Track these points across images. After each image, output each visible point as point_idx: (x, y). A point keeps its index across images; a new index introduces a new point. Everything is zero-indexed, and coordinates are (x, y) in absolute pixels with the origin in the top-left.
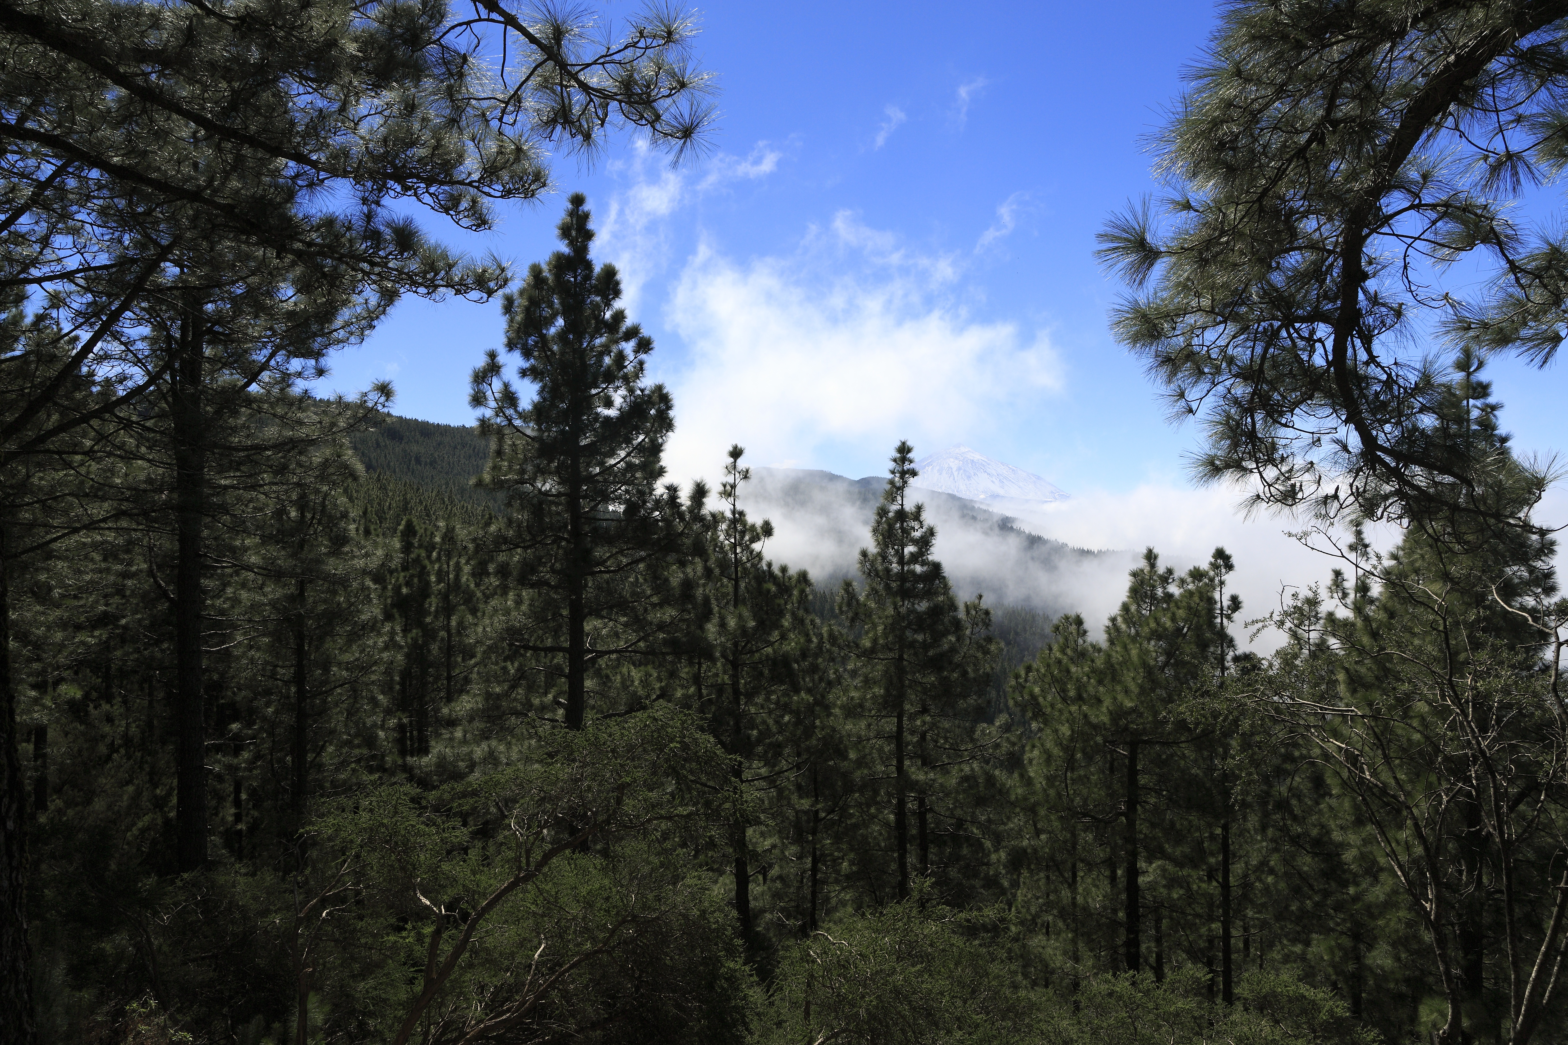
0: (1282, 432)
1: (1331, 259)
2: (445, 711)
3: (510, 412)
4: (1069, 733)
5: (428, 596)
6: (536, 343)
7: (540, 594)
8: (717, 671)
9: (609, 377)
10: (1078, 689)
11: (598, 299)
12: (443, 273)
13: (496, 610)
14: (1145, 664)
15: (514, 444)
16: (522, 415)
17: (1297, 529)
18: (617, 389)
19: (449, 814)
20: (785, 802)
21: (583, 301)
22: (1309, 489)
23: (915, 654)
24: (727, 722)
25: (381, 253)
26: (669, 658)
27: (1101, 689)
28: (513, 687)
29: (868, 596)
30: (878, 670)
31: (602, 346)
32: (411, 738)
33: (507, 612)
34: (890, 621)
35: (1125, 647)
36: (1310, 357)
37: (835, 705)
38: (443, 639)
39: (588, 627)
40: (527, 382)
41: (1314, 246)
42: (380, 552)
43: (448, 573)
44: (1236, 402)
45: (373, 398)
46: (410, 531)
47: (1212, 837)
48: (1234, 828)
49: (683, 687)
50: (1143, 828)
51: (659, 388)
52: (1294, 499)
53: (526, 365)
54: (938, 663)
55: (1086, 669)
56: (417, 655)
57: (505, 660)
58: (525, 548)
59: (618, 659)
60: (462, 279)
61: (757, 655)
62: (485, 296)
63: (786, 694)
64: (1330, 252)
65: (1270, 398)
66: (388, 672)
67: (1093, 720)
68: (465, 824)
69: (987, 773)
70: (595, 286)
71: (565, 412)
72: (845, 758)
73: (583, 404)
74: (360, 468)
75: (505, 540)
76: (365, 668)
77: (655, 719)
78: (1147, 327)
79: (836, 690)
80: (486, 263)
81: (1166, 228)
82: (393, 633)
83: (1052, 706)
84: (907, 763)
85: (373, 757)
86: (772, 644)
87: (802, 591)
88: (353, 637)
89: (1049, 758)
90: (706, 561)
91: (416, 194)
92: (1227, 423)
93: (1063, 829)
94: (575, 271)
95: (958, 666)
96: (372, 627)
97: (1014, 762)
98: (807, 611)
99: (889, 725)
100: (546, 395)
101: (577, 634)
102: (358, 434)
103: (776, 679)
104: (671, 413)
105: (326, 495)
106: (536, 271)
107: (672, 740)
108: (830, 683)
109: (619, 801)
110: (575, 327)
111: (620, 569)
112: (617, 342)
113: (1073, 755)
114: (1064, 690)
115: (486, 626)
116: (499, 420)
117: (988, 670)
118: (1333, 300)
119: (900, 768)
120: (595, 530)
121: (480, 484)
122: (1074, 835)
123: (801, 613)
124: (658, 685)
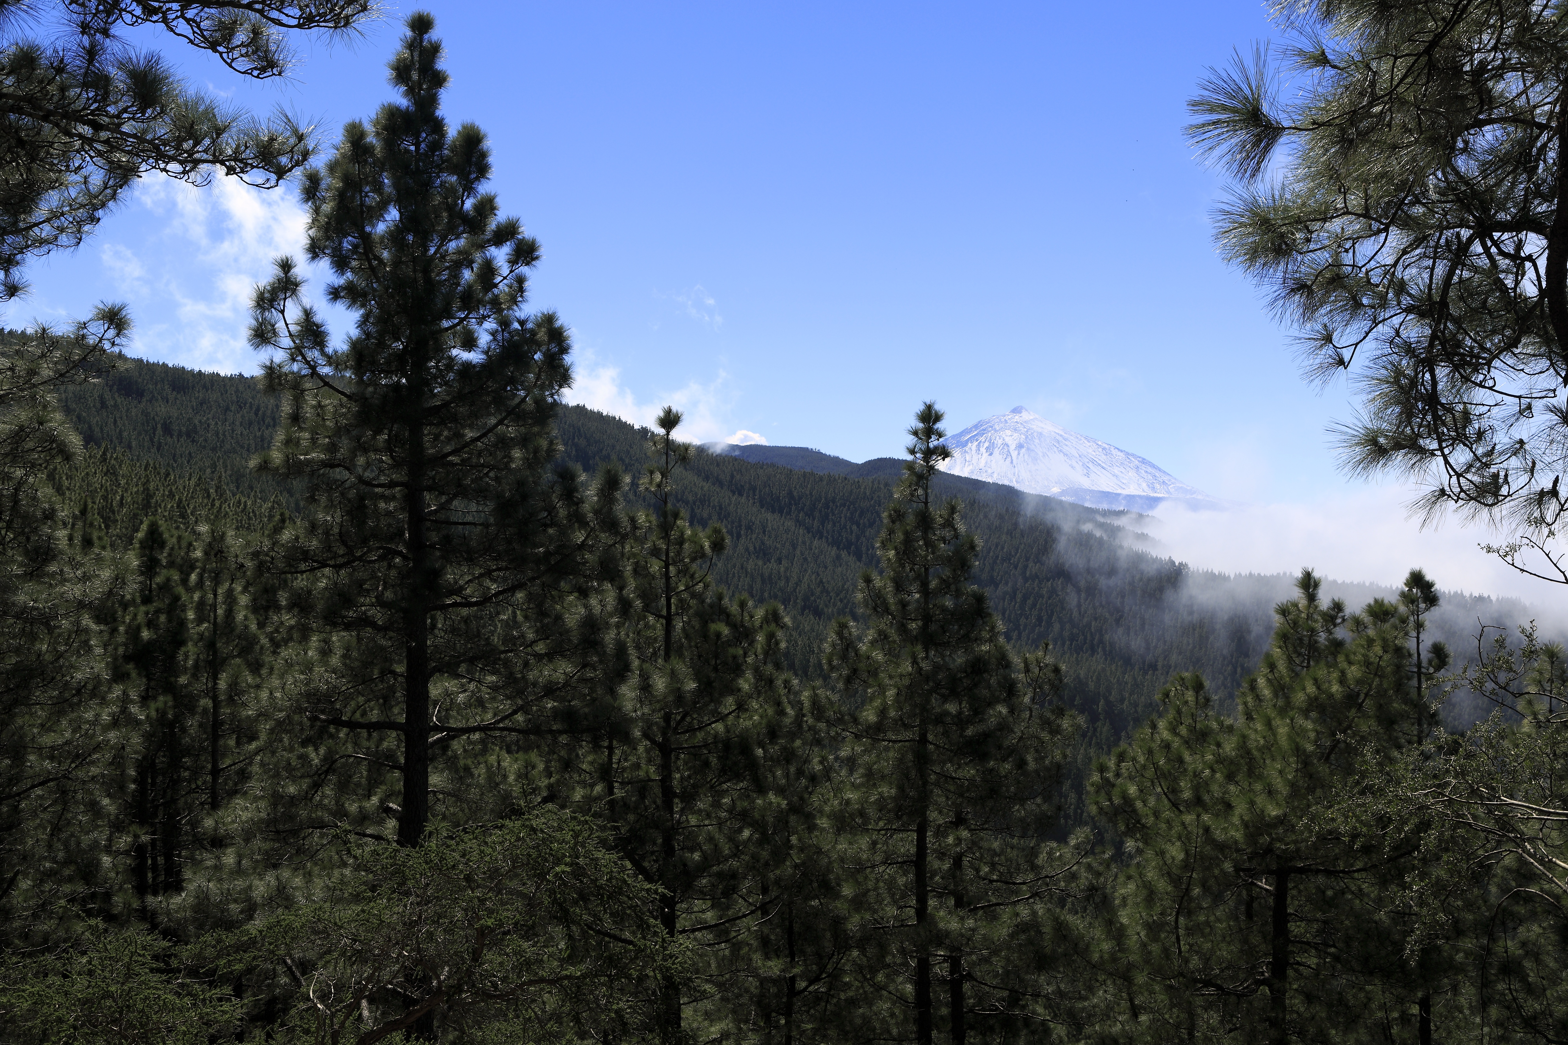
0: (1480, 395)
1: (1544, 137)
2: (209, 823)
3: (313, 354)
4: (1182, 856)
5: (182, 643)
6: (355, 246)
7: (359, 639)
8: (639, 760)
9: (469, 301)
10: (1196, 789)
11: (454, 179)
12: (207, 142)
13: (289, 664)
14: (1298, 750)
15: (319, 405)
16: (330, 360)
17: (1500, 541)
18: (482, 320)
19: (212, 979)
20: (742, 965)
21: (427, 184)
22: (1518, 481)
23: (946, 734)
24: (646, 833)
25: (112, 110)
26: (563, 739)
27: (1232, 788)
28: (316, 786)
29: (873, 643)
30: (887, 759)
31: (459, 252)
32: (155, 867)
33: (308, 667)
34: (906, 681)
35: (1268, 723)
36: (1517, 283)
37: (821, 812)
38: (205, 710)
39: (435, 690)
40: (340, 307)
41: (1521, 118)
42: (106, 574)
43: (214, 607)
44: (1409, 349)
45: (96, 331)
46: (154, 540)
47: (1405, 1019)
48: (1439, 1006)
49: (583, 784)
50: (1295, 1002)
51: (549, 320)
52: (1496, 494)
53: (339, 281)
54: (978, 749)
55: (1209, 757)
56: (165, 736)
57: (304, 744)
58: (337, 567)
59: (482, 741)
60: (236, 151)
61: (700, 735)
62: (273, 177)
63: (745, 795)
64: (1542, 127)
65: (1459, 344)
66: (118, 761)
67: (1219, 835)
68: (239, 992)
69: (1056, 919)
70: (449, 160)
71: (400, 357)
72: (837, 896)
73: (426, 344)
74: (74, 440)
75: (306, 555)
76: (81, 758)
77: (534, 830)
78: (1270, 237)
79: (825, 789)
80: (274, 127)
81: (1291, 92)
82: (125, 700)
83: (1156, 814)
84: (932, 903)
85: (93, 896)
86: (722, 718)
87: (771, 636)
88: (63, 706)
89: (1150, 896)
90: (621, 589)
91: (165, 21)
92: (1397, 381)
93: (1172, 1006)
94: (418, 136)
95: (1012, 751)
96: (93, 690)
97: (1098, 901)
98: (778, 666)
99: (905, 844)
100: (371, 329)
101: (418, 701)
102: (71, 388)
103: (729, 772)
104: (568, 359)
105: (21, 483)
106: (355, 134)
107: (558, 861)
108: (813, 779)
109: (476, 956)
110: (416, 224)
111: (486, 600)
112: (482, 247)
113: (1188, 890)
114: (1174, 791)
115: (273, 690)
116: (295, 367)
117: (1058, 757)
118: (1545, 199)
119: (921, 912)
120: (447, 539)
121: (264, 466)
122: (1192, 1016)
123: (769, 669)
124: (544, 782)
